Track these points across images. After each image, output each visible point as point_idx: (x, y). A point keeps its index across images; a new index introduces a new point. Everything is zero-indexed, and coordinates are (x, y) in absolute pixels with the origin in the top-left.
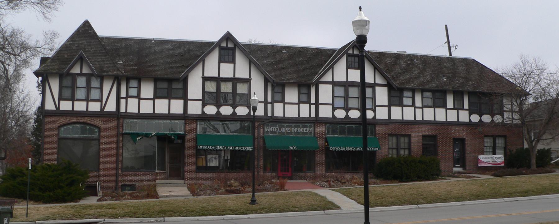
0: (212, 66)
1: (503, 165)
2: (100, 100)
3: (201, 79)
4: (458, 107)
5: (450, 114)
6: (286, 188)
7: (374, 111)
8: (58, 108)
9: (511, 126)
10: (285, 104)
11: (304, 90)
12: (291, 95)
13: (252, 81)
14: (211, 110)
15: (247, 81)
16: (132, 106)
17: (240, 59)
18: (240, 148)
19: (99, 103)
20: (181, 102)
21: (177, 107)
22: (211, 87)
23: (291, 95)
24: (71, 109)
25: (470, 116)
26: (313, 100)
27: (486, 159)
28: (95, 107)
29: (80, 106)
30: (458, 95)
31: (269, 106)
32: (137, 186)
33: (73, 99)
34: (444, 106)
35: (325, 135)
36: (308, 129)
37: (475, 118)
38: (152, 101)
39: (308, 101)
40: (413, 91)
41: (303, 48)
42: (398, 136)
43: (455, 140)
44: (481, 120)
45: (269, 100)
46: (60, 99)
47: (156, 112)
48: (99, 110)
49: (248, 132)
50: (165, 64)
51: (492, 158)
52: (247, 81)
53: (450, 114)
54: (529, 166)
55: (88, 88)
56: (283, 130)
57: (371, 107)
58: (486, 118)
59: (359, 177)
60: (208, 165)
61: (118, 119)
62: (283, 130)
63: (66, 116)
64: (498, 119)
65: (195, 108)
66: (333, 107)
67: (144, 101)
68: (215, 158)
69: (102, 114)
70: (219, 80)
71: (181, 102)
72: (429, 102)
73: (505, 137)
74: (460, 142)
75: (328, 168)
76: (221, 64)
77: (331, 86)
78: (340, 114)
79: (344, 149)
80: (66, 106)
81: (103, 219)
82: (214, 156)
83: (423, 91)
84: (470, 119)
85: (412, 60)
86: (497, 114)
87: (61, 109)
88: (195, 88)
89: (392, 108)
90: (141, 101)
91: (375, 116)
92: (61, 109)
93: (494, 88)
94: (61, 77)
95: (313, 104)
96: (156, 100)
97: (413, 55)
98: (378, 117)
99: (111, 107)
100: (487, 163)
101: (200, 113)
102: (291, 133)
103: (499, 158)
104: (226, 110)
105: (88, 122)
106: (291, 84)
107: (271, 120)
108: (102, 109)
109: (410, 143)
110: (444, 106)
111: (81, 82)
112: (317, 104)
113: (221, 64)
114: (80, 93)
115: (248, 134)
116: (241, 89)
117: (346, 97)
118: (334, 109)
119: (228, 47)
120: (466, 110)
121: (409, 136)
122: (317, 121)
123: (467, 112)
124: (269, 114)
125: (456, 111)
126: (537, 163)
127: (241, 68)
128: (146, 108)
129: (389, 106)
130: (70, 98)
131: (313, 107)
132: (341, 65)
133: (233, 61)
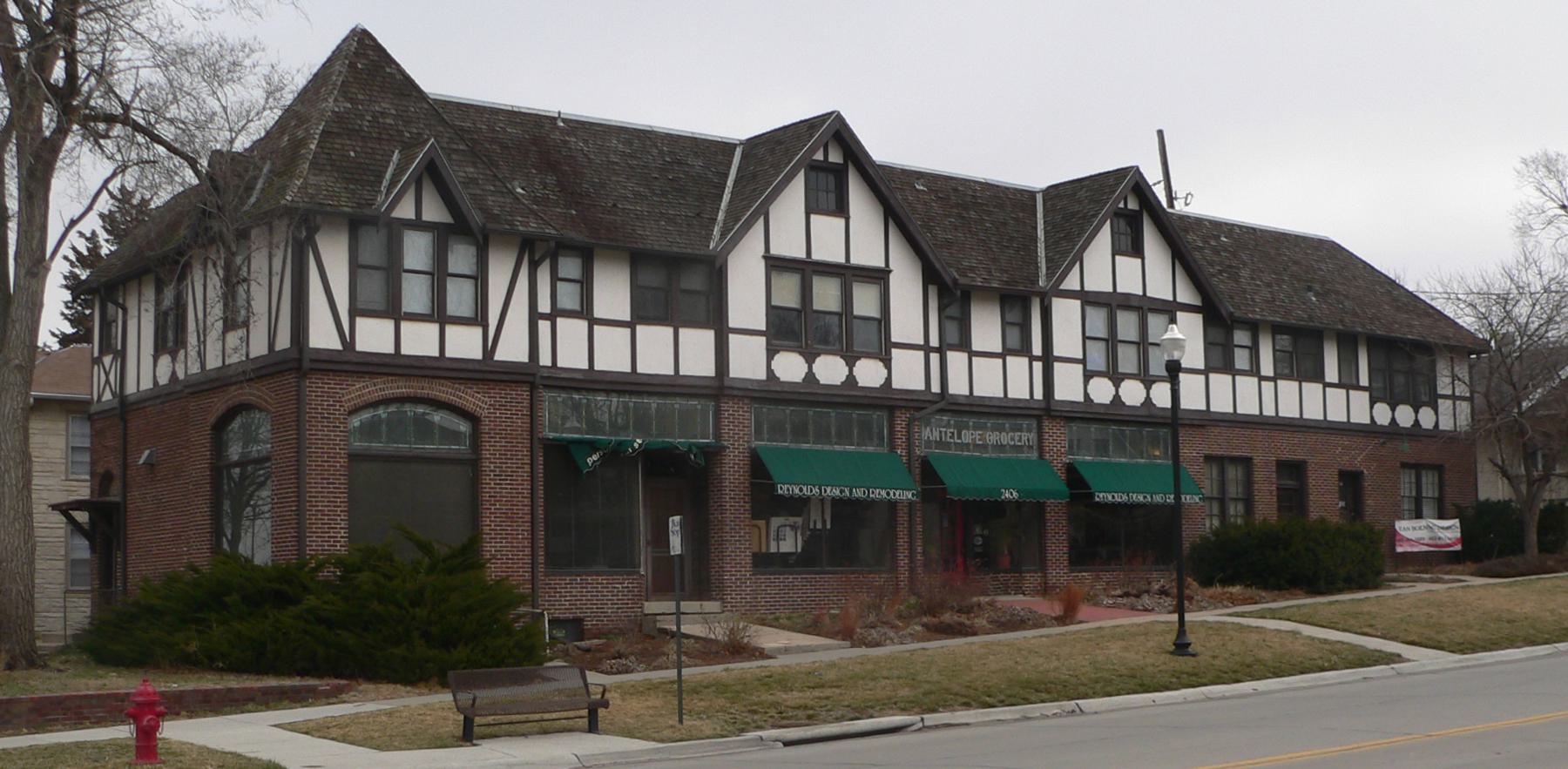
0: (790, 224)
1: (1458, 547)
2: (478, 318)
3: (762, 263)
4: (1348, 383)
5: (1331, 401)
6: (1080, 616)
8: (348, 343)
9: (1451, 438)
10: (593, 322)
11: (1014, 316)
12: (987, 329)
13: (891, 276)
14: (790, 367)
15: (879, 277)
16: (570, 348)
17: (858, 199)
18: (884, 493)
19: (478, 331)
20: (707, 337)
21: (696, 353)
22: (788, 293)
23: (987, 329)
24: (390, 349)
25: (770, 358)
26: (1037, 350)
27: (1415, 533)
28: (464, 344)
29: (420, 340)
30: (1348, 344)
31: (544, 326)
32: (588, 624)
33: (393, 311)
34: (1317, 376)
35: (1071, 450)
36: (1025, 436)
37: (1382, 414)
38: (627, 331)
39: (1024, 350)
40: (1254, 328)
42: (1418, 468)
43: (1343, 475)
44: (810, 376)
46: (354, 312)
48: (478, 355)
49: (881, 444)
50: (627, 202)
51: (1428, 527)
52: (879, 277)
53: (1331, 401)
54: (1520, 549)
55: (439, 275)
56: (967, 437)
57: (1133, 369)
58: (1405, 416)
59: (1161, 580)
60: (773, 549)
61: (533, 387)
62: (967, 437)
63: (373, 374)
64: (1427, 418)
65: (748, 359)
67: (609, 336)
68: (794, 527)
69: (486, 372)
70: (807, 269)
71: (707, 337)
73: (1439, 469)
74: (1351, 482)
75: (1081, 557)
77: (1078, 303)
78: (1102, 391)
79: (1125, 498)
80: (374, 336)
81: (918, 718)
82: (792, 520)
83: (1276, 330)
84: (1086, 394)
85: (1217, 238)
86: (869, 356)
87: (359, 348)
88: (747, 295)
90: (974, 359)
91: (889, 379)
92: (359, 348)
93: (1415, 331)
94: (356, 225)
95: (1037, 359)
96: (639, 328)
97: (1210, 222)
99: (512, 349)
100: (1418, 542)
101: (762, 375)
102: (984, 447)
103: (1448, 531)
104: (831, 370)
105: (443, 396)
106: (986, 293)
107: (941, 405)
108: (489, 351)
109: (1249, 483)
110: (1317, 376)
111: (417, 251)
112: (1048, 359)
113: (813, 217)
114: (415, 294)
115: (880, 450)
116: (865, 301)
117: (1112, 342)
118: (1088, 375)
119: (824, 156)
120: (1363, 389)
121: (1246, 462)
122: (1046, 411)
123: (1366, 395)
124: (545, 359)
125: (1344, 391)
126: (1540, 542)
127: (861, 235)
128: (612, 355)
130: (380, 307)
131: (1038, 366)
132: (791, 204)
133: (840, 209)
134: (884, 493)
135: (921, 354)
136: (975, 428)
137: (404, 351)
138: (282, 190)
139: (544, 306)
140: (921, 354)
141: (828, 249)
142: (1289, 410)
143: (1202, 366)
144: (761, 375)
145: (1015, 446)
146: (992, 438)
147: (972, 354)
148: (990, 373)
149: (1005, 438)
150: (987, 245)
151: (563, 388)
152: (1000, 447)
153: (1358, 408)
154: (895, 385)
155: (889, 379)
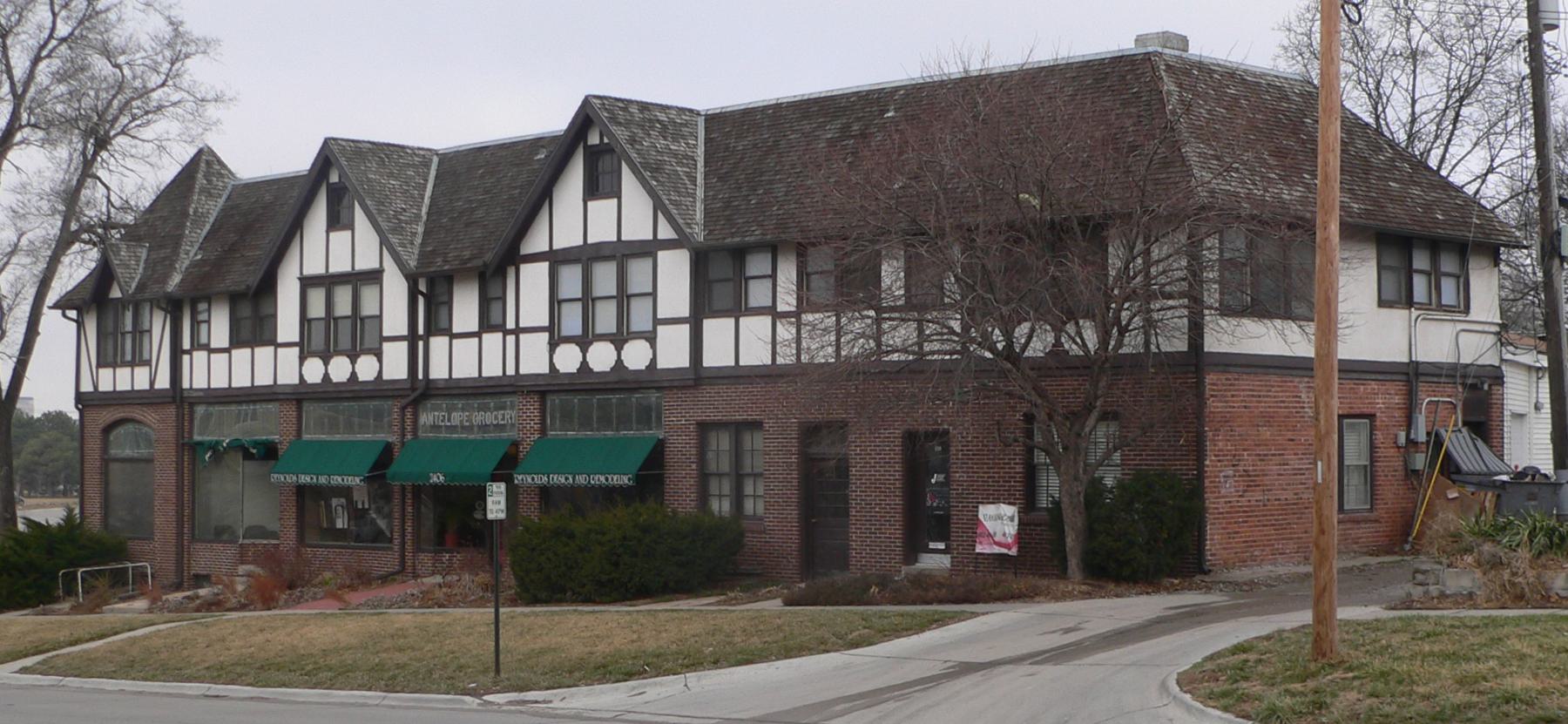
4: (916, 306)
7: (651, 338)
12: (465, 309)
18: (602, 479)
26: (511, 324)
41: (481, 150)
45: (421, 331)
46: (99, 366)
47: (742, 363)
52: (374, 276)
66: (301, 352)
72: (821, 288)
76: (332, 235)
78: (568, 359)
89: (280, 340)
91: (654, 360)
98: (387, 375)
102: (470, 429)
129: (695, 322)
134: (602, 479)
135: (522, 337)
136: (463, 410)
137: (742, 363)
138: (164, 279)
139: (186, 345)
140: (522, 337)
141: (602, 230)
142: (241, 380)
143: (476, 329)
144: (546, 370)
145: (497, 426)
146: (479, 418)
147: (453, 336)
148: (460, 357)
149: (489, 418)
150: (473, 217)
151: (475, 395)
152: (484, 428)
153: (823, 341)
154: (386, 377)
155: (654, 360)
